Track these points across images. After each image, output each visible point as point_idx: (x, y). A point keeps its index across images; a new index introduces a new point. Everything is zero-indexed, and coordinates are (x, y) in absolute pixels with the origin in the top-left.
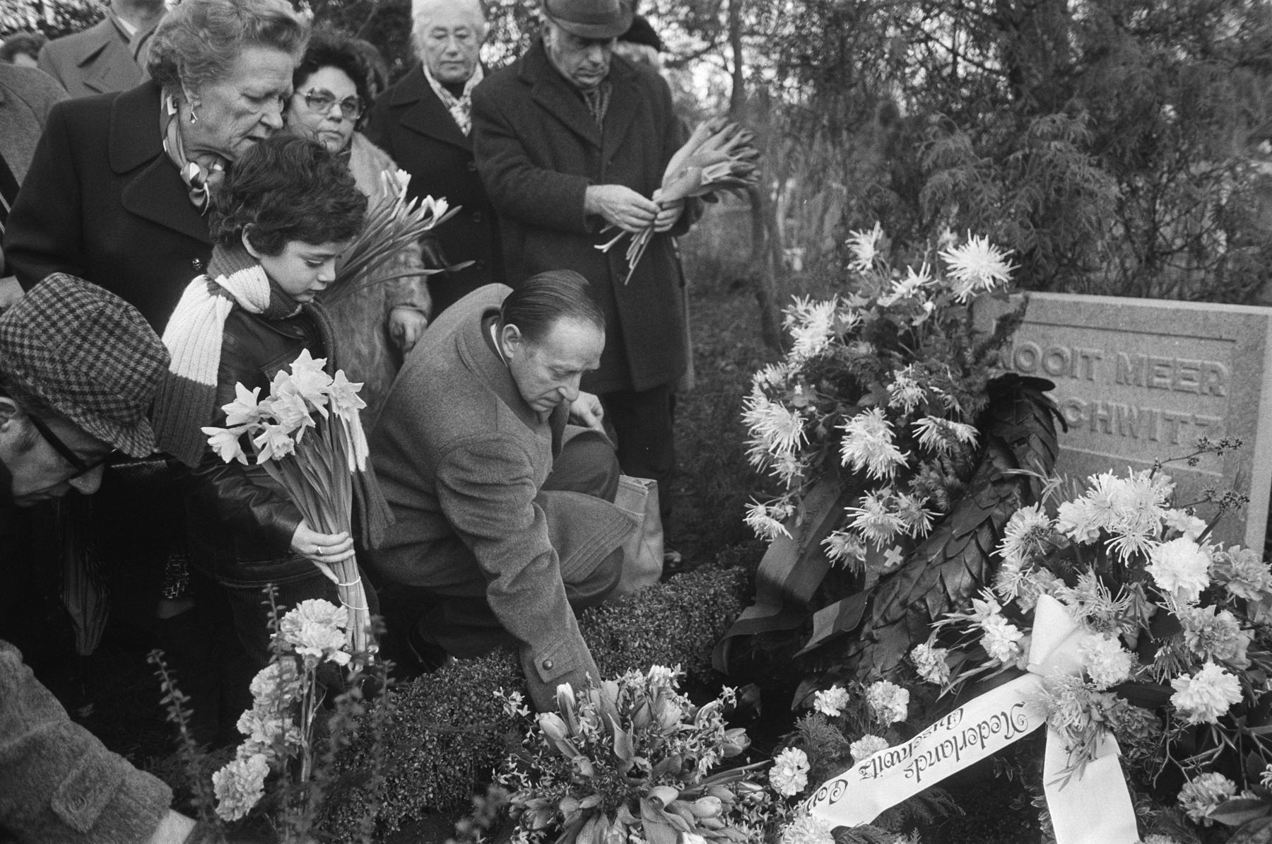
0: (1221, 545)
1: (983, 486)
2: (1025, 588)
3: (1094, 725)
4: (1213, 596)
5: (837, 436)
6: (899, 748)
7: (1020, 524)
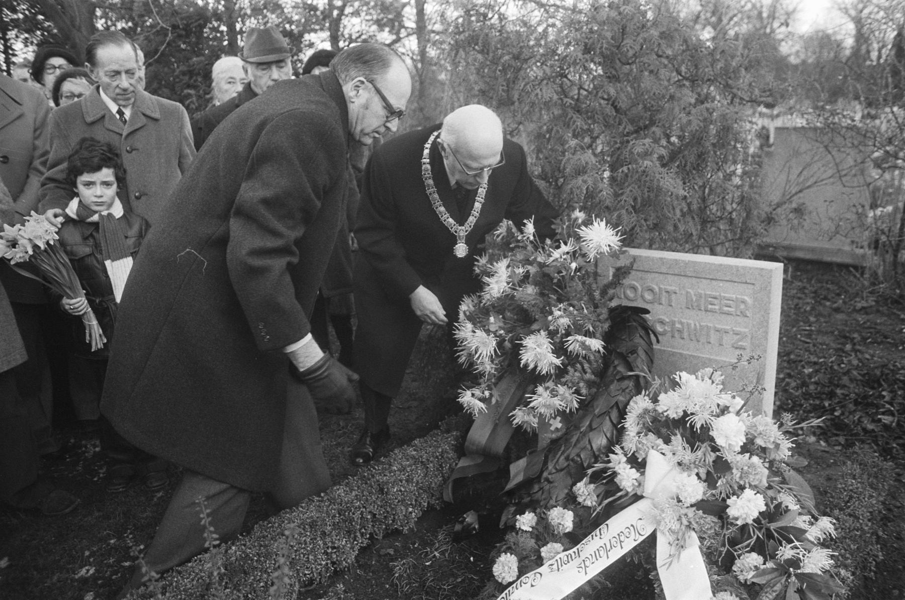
0: (750, 413)
1: (612, 382)
2: (640, 446)
3: (683, 527)
4: (748, 448)
5: (517, 349)
6: (571, 551)
7: (635, 406)
